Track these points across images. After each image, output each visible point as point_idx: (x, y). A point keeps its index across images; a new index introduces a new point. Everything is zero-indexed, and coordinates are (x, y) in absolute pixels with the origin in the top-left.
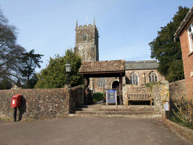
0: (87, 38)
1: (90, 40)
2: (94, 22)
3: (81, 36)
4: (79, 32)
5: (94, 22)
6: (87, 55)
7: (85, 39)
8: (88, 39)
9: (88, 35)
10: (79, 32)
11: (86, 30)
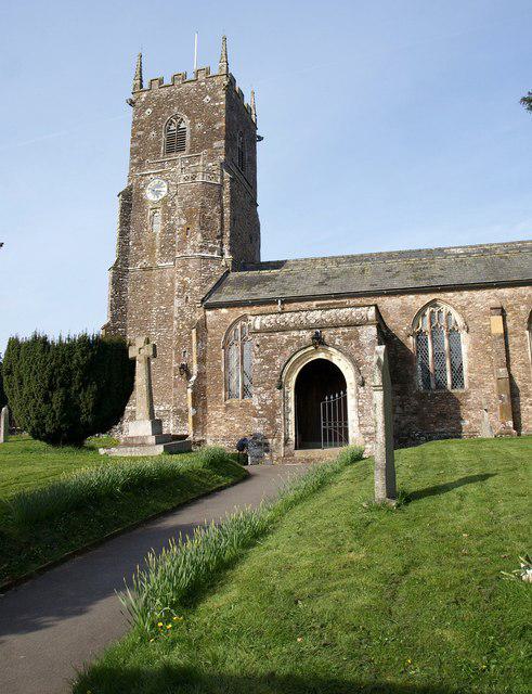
6: (183, 222)
8: (193, 145)
9: (193, 124)
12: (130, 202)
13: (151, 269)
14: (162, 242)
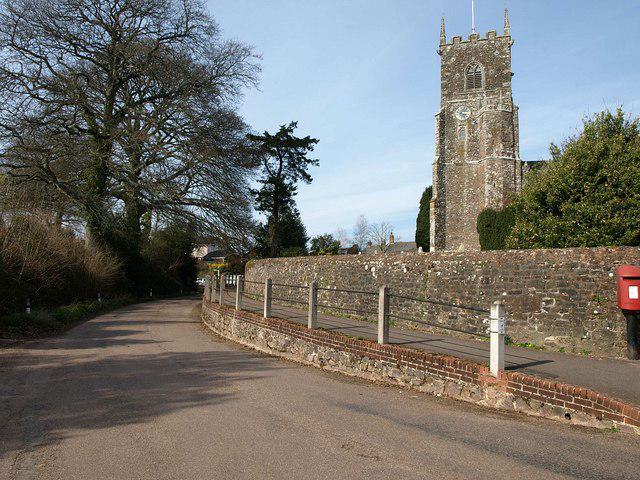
0: (483, 77)
1: (496, 85)
3: (460, 71)
4: (453, 59)
6: (490, 136)
7: (474, 82)
8: (488, 83)
9: (487, 70)
10: (453, 59)
11: (476, 52)
12: (445, 121)
13: (462, 165)
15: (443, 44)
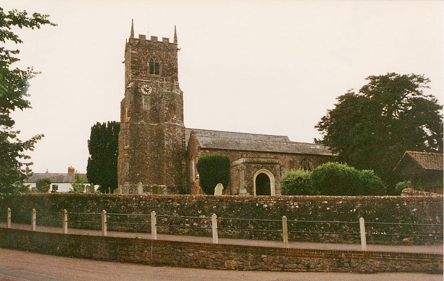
2: (176, 37)
5: (176, 37)
8: (163, 72)
14: (150, 114)
15: (132, 38)
